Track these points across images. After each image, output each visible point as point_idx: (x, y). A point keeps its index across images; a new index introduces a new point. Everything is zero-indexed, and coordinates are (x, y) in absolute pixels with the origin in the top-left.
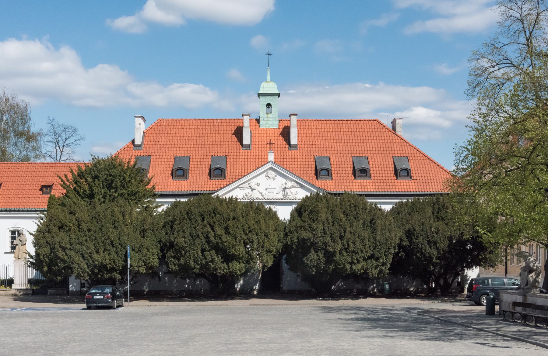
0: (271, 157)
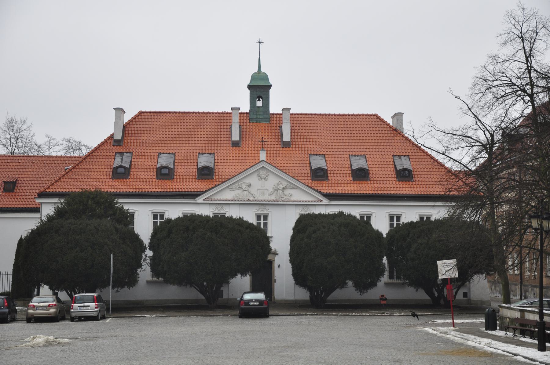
0: (263, 156)
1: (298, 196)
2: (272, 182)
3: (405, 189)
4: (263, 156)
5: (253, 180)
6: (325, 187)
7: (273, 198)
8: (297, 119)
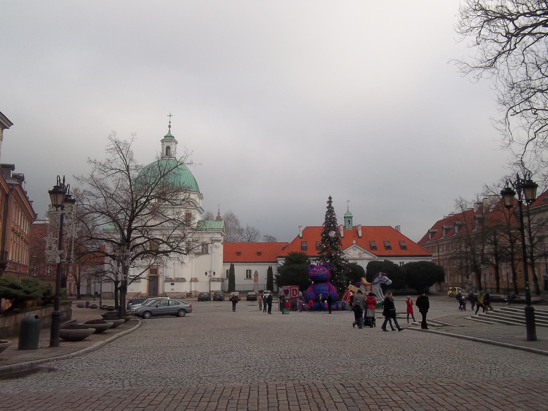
0: (354, 242)
1: (367, 256)
2: (358, 251)
3: (404, 252)
4: (354, 242)
5: (351, 251)
6: (377, 252)
7: (358, 257)
8: (363, 228)
